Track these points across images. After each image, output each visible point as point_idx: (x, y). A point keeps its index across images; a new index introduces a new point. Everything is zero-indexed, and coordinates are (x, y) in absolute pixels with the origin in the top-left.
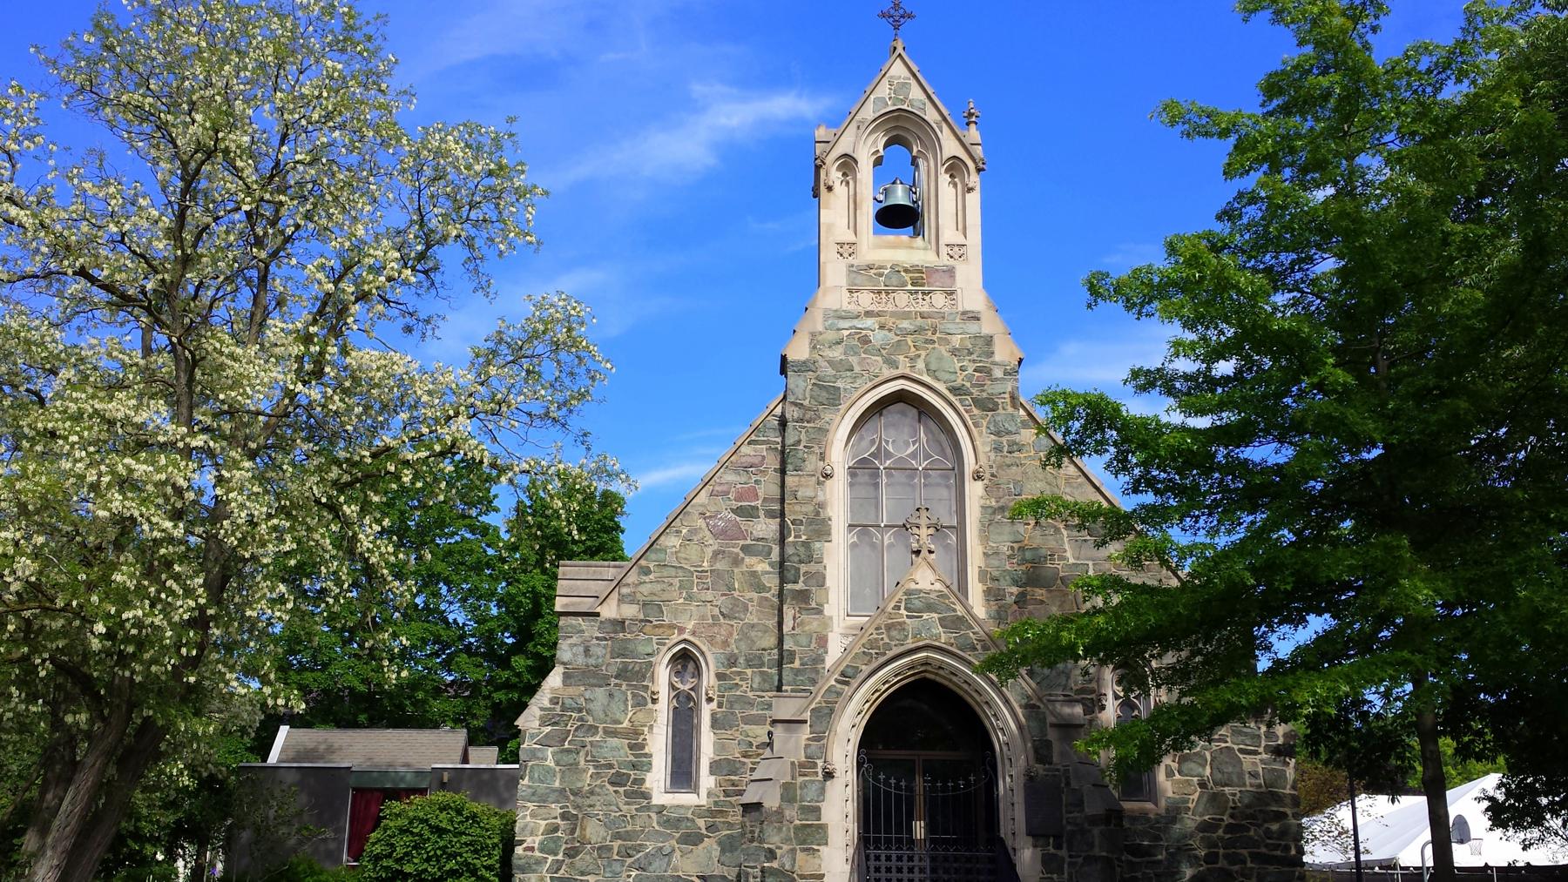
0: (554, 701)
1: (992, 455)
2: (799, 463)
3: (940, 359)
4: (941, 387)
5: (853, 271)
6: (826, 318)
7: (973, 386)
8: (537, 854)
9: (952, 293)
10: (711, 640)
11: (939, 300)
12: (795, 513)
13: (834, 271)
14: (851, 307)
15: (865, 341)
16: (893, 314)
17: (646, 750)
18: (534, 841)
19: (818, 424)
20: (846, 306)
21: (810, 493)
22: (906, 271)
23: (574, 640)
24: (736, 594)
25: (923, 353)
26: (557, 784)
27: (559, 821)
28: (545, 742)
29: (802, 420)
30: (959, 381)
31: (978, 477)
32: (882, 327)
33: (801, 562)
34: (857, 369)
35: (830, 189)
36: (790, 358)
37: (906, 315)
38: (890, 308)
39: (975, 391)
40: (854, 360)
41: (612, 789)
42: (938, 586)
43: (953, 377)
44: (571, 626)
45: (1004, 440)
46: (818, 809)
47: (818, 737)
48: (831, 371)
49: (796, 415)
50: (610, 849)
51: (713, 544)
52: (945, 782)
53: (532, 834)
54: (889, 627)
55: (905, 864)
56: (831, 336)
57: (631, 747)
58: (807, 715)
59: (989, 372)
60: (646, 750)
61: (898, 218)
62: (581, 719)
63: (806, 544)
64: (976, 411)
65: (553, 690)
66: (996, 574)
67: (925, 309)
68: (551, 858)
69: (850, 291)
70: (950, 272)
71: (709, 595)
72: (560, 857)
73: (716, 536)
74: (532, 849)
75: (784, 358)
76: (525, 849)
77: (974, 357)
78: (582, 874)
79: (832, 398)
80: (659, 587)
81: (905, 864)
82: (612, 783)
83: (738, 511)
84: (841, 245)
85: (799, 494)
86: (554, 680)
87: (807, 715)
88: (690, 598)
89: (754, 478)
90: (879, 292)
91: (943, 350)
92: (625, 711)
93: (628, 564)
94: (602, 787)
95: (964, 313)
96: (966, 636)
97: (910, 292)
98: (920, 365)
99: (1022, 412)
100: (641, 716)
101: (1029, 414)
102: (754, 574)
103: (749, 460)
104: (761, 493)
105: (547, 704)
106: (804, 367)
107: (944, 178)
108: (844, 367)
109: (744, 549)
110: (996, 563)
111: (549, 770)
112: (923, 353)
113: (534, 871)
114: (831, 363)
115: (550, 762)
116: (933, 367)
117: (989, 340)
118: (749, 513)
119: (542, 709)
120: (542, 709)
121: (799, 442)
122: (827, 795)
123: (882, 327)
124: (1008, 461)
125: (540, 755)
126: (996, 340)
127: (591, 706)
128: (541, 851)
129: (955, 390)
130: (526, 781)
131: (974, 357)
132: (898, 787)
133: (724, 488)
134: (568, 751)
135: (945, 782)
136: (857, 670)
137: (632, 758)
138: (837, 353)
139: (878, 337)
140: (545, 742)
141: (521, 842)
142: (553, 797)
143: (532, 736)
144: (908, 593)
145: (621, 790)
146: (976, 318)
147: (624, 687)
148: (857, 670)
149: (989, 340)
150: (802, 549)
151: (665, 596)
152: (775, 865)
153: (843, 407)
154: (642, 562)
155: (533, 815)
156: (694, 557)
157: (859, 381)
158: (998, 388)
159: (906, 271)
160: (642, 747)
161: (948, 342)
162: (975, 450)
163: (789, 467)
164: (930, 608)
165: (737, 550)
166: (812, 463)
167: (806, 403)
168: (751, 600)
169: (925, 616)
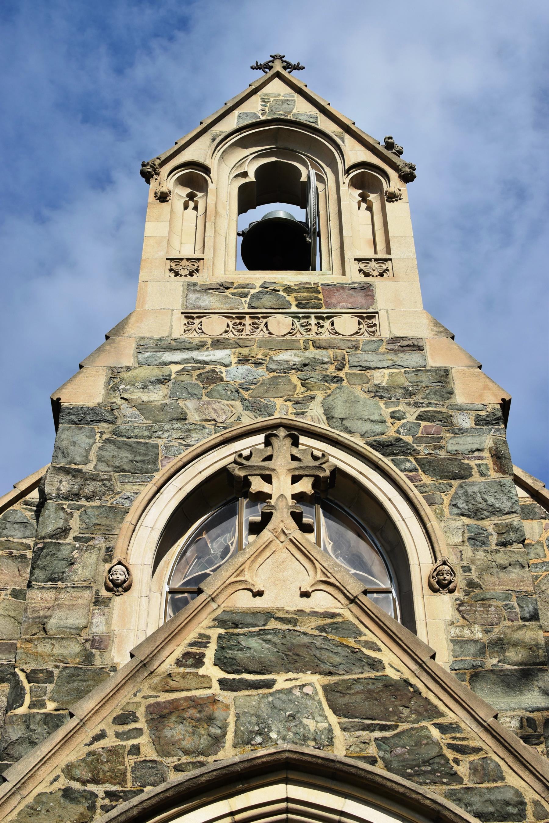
4: (358, 442)
6: (141, 348)
7: (419, 440)
9: (371, 316)
14: (194, 337)
19: (109, 501)
21: (75, 619)
29: (76, 496)
31: (440, 584)
34: (194, 417)
36: (65, 403)
39: (424, 450)
42: (323, 601)
43: (378, 428)
45: (488, 524)
48: (142, 421)
49: (65, 487)
54: (160, 716)
59: (446, 421)
64: (426, 479)
67: (326, 336)
75: (56, 405)
77: (418, 398)
79: (143, 462)
84: (178, 260)
85: (52, 623)
90: (241, 316)
95: (393, 341)
96: (421, 740)
97: (295, 315)
101: (535, 494)
106: (86, 417)
107: (350, 196)
114: (143, 408)
116: (339, 413)
117: (444, 375)
121: (65, 531)
123: (243, 361)
124: (501, 558)
126: (454, 373)
129: (382, 447)
131: (418, 398)
138: (158, 396)
139: (235, 374)
144: (230, 621)
146: (416, 347)
149: (444, 375)
153: (158, 477)
158: (466, 443)
164: (294, 658)
166: (89, 566)
169: (281, 681)
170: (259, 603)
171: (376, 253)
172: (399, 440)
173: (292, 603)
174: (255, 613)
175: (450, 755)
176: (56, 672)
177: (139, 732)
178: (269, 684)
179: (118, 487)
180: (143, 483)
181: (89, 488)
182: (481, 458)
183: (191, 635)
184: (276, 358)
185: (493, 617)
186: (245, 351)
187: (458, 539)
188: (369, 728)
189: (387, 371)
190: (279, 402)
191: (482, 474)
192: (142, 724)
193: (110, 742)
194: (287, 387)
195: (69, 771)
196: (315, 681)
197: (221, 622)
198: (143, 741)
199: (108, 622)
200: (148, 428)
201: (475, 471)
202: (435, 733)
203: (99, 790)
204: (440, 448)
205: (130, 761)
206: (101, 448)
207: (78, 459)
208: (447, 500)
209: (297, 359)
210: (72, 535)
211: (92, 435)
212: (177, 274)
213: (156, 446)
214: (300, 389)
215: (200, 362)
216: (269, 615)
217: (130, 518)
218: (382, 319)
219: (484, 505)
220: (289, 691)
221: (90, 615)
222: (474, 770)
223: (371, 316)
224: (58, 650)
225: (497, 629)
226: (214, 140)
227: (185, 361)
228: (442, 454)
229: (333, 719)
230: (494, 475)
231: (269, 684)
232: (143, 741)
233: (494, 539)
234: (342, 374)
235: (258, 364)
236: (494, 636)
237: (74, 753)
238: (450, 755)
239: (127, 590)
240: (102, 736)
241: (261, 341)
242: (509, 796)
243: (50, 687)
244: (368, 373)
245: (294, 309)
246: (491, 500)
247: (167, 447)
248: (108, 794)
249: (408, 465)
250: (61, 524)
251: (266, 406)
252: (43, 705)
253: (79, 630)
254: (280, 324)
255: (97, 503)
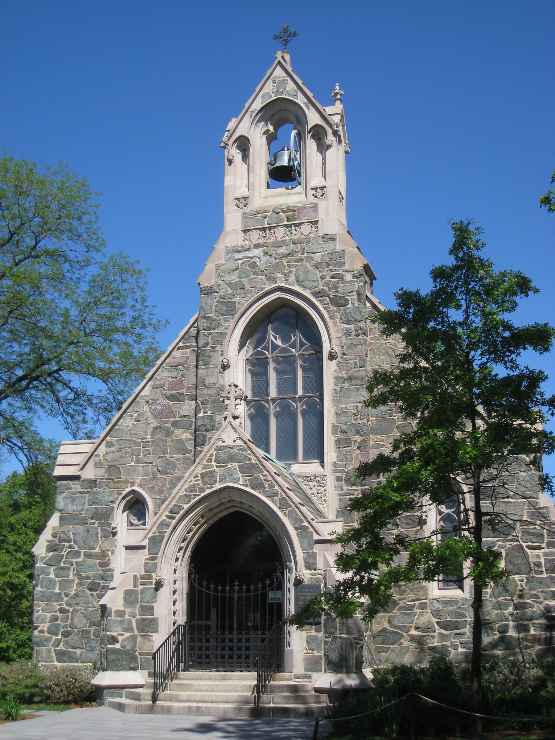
0: (54, 536)
1: (344, 339)
2: (207, 359)
3: (306, 272)
4: (306, 293)
5: (246, 217)
7: (330, 289)
8: (47, 634)
9: (316, 222)
10: (151, 490)
11: (306, 229)
12: (203, 395)
13: (233, 219)
15: (254, 266)
16: (274, 244)
17: (111, 567)
18: (44, 626)
20: (241, 243)
21: (213, 380)
22: (283, 211)
23: (65, 495)
24: (168, 456)
25: (294, 269)
26: (57, 590)
27: (58, 614)
28: (49, 564)
29: (209, 329)
30: (320, 287)
31: (332, 357)
32: (266, 254)
33: (207, 430)
34: (247, 286)
35: (230, 162)
37: (282, 243)
38: (273, 239)
40: (245, 281)
41: (89, 592)
44: (64, 485)
46: (152, 608)
47: (153, 558)
50: (88, 632)
51: (154, 422)
52: (248, 585)
53: (42, 622)
55: (244, 644)
56: (231, 265)
57: (101, 565)
58: (146, 543)
60: (111, 567)
61: (283, 175)
62: (70, 547)
63: (210, 418)
64: (332, 308)
65: (54, 528)
66: (344, 427)
68: (54, 637)
69: (244, 231)
70: (315, 207)
71: (150, 458)
72: (59, 637)
73: (155, 416)
74: (42, 631)
76: (40, 632)
77: (331, 268)
78: (73, 648)
80: (118, 455)
81: (244, 644)
82: (90, 589)
83: (171, 398)
84: (238, 199)
85: (207, 382)
86: (54, 521)
87: (146, 543)
88: (138, 461)
89: (181, 373)
90: (264, 229)
91: (309, 265)
92: (97, 541)
93: (98, 441)
94: (83, 591)
95: (324, 236)
96: (258, 478)
98: (292, 278)
99: (368, 305)
100: (106, 545)
102: (181, 441)
103: (179, 361)
104: (185, 383)
105: (50, 538)
108: (239, 287)
109: (174, 424)
110: (345, 419)
111: (51, 581)
112: (294, 269)
113: (44, 646)
114: (230, 285)
115: (52, 576)
116: (301, 279)
118: (176, 398)
119: (47, 541)
120: (47, 541)
121: (207, 344)
122: (158, 598)
123: (266, 254)
124: (354, 342)
125: (46, 571)
127: (77, 538)
128: (48, 632)
130: (39, 589)
131: (331, 268)
132: (216, 590)
133: (162, 382)
134: (63, 568)
135: (248, 585)
136: (180, 508)
137: (101, 572)
138: (234, 278)
139: (262, 263)
140: (49, 564)
141: (36, 628)
142: (54, 598)
143: (42, 559)
144: (218, 449)
145: (95, 593)
147: (96, 526)
148: (180, 508)
150: (207, 421)
151: (123, 461)
152: (117, 646)
153: (236, 316)
154: (108, 438)
155: (43, 610)
156: (141, 433)
157: (249, 295)
158: (348, 288)
159: (283, 211)
160: (107, 564)
161: (313, 259)
162: (332, 336)
163: (201, 363)
164: (232, 459)
165: (168, 425)
166: (217, 359)
167: (212, 316)
168: (178, 460)
170: (224, 444)
171: (143, 547)
172: (323, 289)
173: (232, 444)
174: (223, 446)
175: (264, 482)
176: (210, 400)
177: (199, 480)
178: (226, 466)
179: (223, 323)
180: (231, 320)
181: (213, 325)
182: (353, 296)
183: (209, 454)
184: (278, 252)
185: (349, 368)
186: (266, 249)
187: (341, 335)
188: (247, 476)
189: (320, 254)
190: (279, 275)
191: (352, 304)
192: (199, 478)
193: (193, 482)
194: (282, 267)
195: (185, 489)
196: (236, 464)
197: (216, 450)
198: (200, 482)
199: (224, 380)
200: (232, 294)
201: (350, 302)
202: (261, 477)
203: (192, 494)
204: (338, 292)
205: (198, 487)
206: (216, 306)
207: (209, 312)
208: (339, 316)
209: (286, 251)
210: (210, 345)
211: (212, 300)
212: (239, 207)
213: (235, 303)
214: (287, 268)
215: (249, 258)
216: (226, 447)
217: (228, 337)
218: (320, 224)
219: (351, 319)
220: (230, 468)
221: (218, 378)
222: (269, 485)
223: (316, 222)
224: (209, 392)
225: (350, 372)
226: (251, 116)
227: (244, 258)
228: (339, 295)
229: (240, 475)
230: (357, 304)
231: (226, 466)
232: (200, 482)
233: (353, 333)
234: (303, 257)
235: (271, 256)
236: (349, 375)
237: (186, 486)
238: (264, 482)
239: (229, 368)
240: (191, 481)
241: (272, 243)
242: (275, 492)
243: (209, 405)
244: (313, 255)
245: (286, 223)
246: (354, 315)
247: (239, 303)
248: (194, 495)
249: (325, 302)
250: (205, 342)
251: (274, 278)
252: (207, 412)
253: (215, 384)
254: (280, 232)
255: (216, 331)
